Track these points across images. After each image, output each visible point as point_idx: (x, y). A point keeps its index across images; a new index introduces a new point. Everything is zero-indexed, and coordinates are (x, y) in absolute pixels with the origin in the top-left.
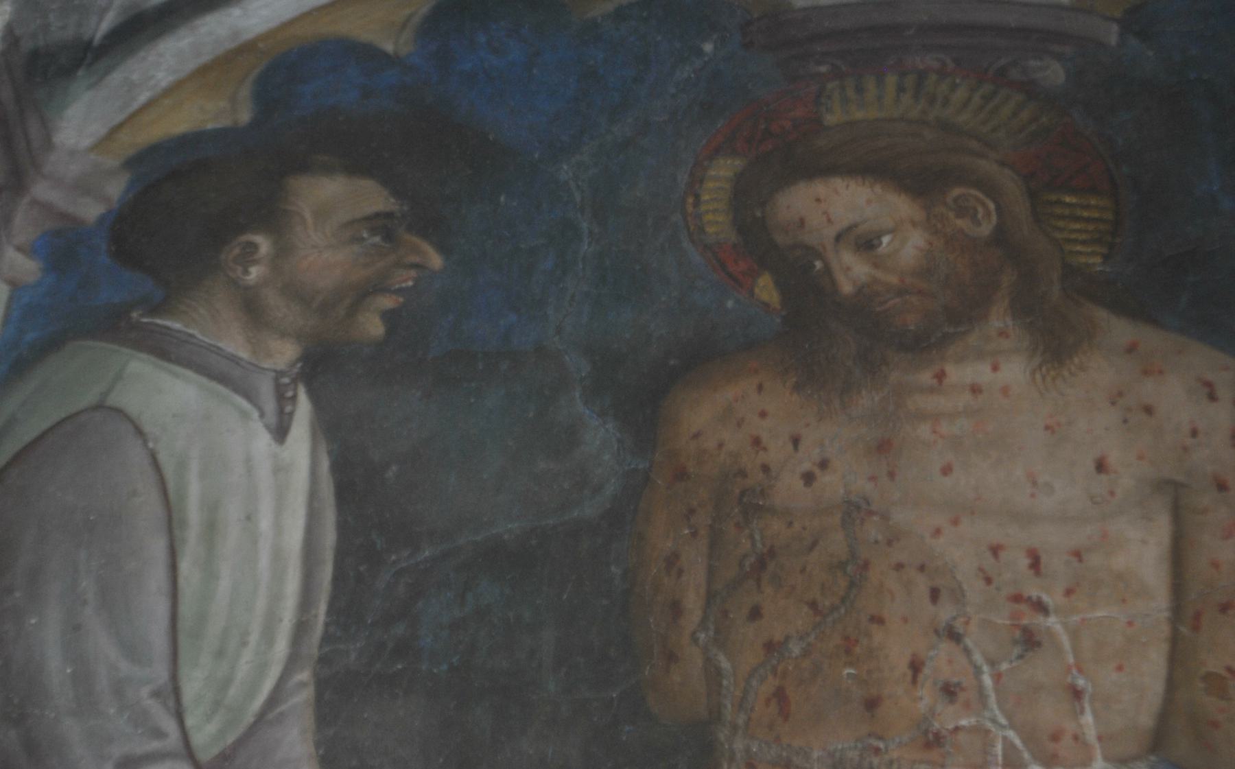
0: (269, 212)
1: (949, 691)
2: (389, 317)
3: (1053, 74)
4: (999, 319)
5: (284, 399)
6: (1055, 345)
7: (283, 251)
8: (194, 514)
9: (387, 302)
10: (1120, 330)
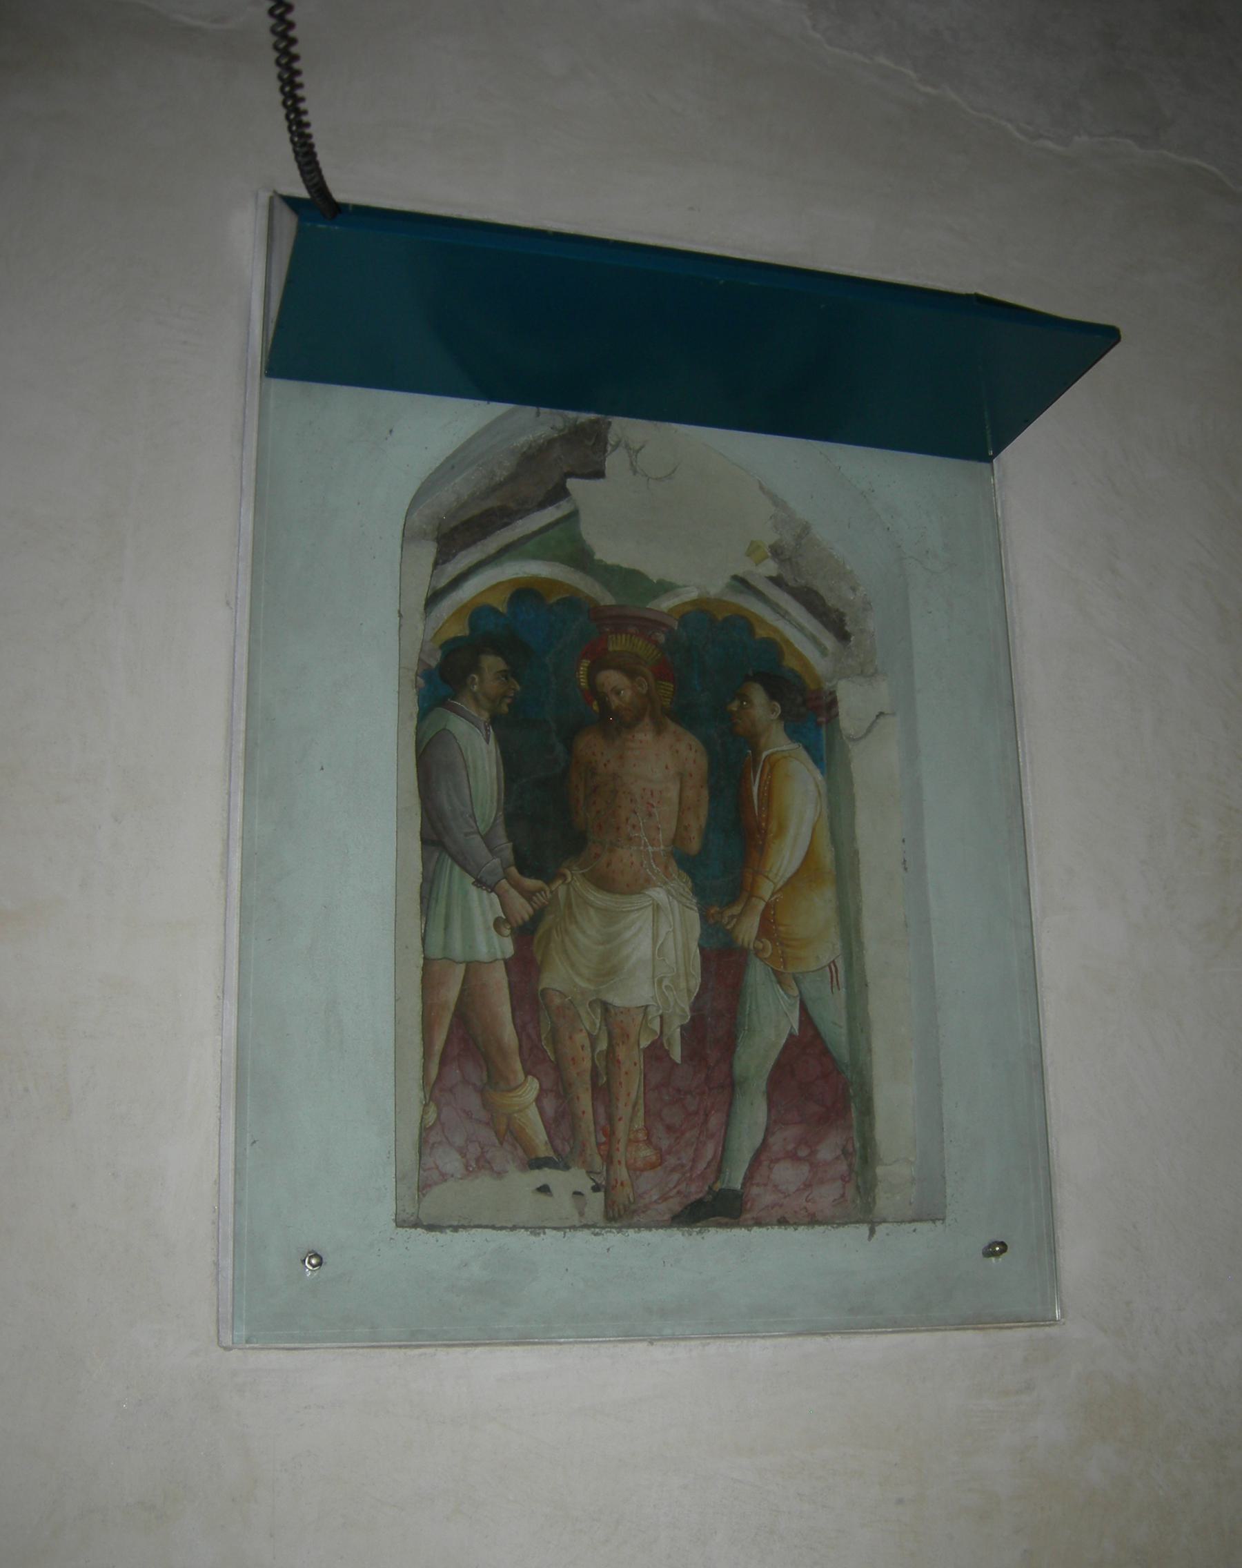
0: (475, 667)
1: (634, 826)
2: (509, 705)
3: (662, 638)
4: (647, 720)
5: (487, 731)
6: (659, 730)
7: (482, 681)
8: (470, 764)
9: (508, 701)
10: (672, 726)
